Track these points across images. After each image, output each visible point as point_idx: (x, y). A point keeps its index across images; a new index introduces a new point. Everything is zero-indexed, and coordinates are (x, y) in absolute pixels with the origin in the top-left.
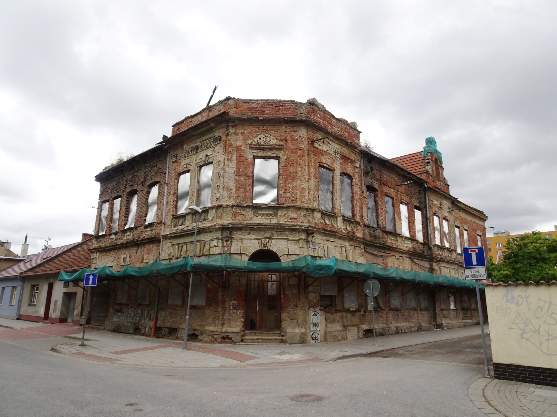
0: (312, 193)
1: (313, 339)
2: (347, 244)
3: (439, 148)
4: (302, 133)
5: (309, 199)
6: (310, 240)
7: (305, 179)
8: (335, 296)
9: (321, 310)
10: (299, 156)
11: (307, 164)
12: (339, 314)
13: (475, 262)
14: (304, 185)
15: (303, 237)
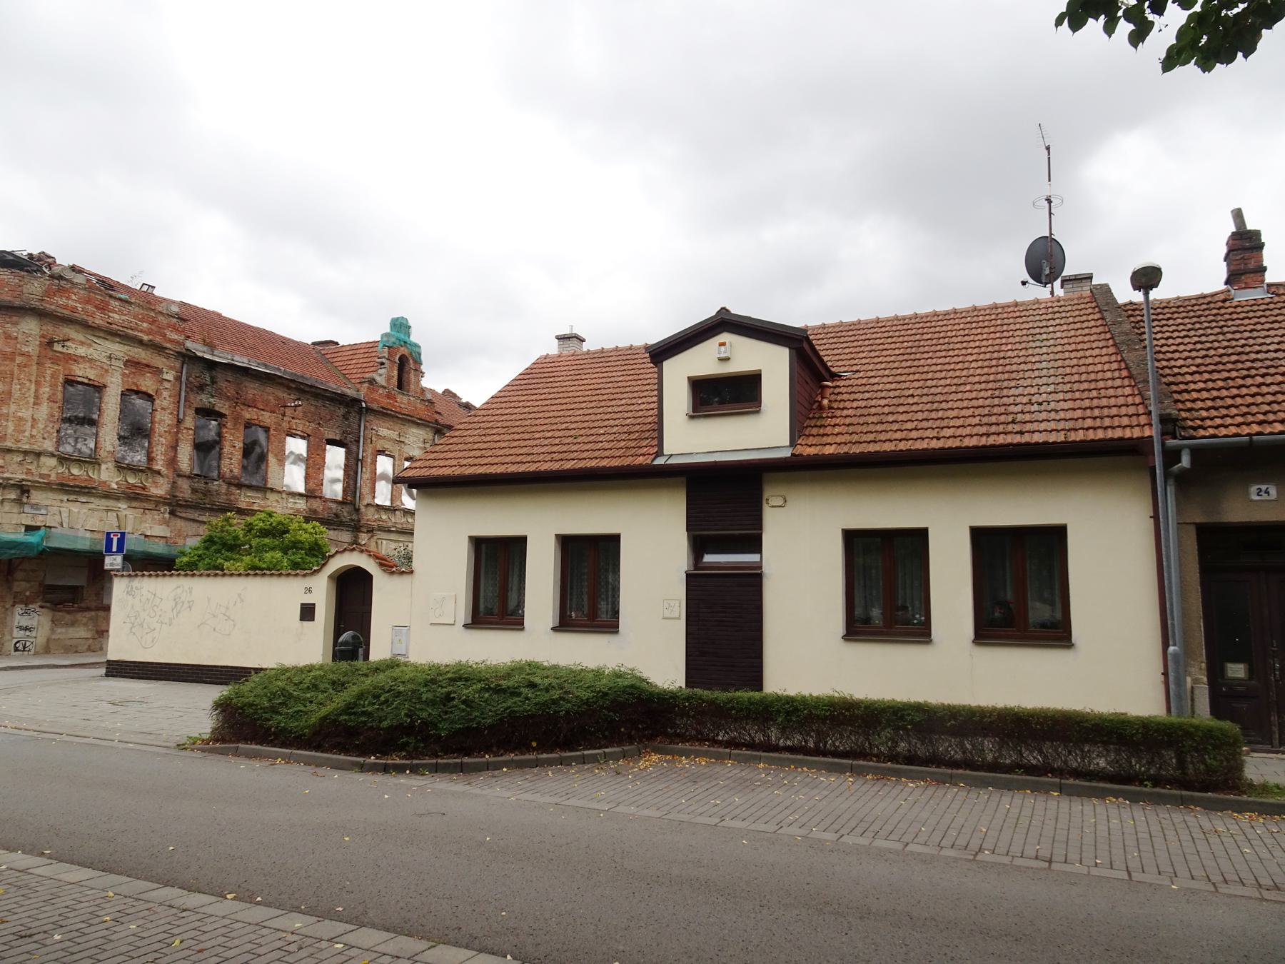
0: (41, 426)
1: (16, 650)
2: (123, 505)
3: (414, 338)
4: (30, 327)
5: (32, 436)
6: (25, 500)
7: (28, 403)
8: (82, 587)
9: (41, 607)
10: (19, 365)
11: (33, 379)
12: (88, 614)
13: (114, 549)
14: (25, 413)
15: (13, 496)
